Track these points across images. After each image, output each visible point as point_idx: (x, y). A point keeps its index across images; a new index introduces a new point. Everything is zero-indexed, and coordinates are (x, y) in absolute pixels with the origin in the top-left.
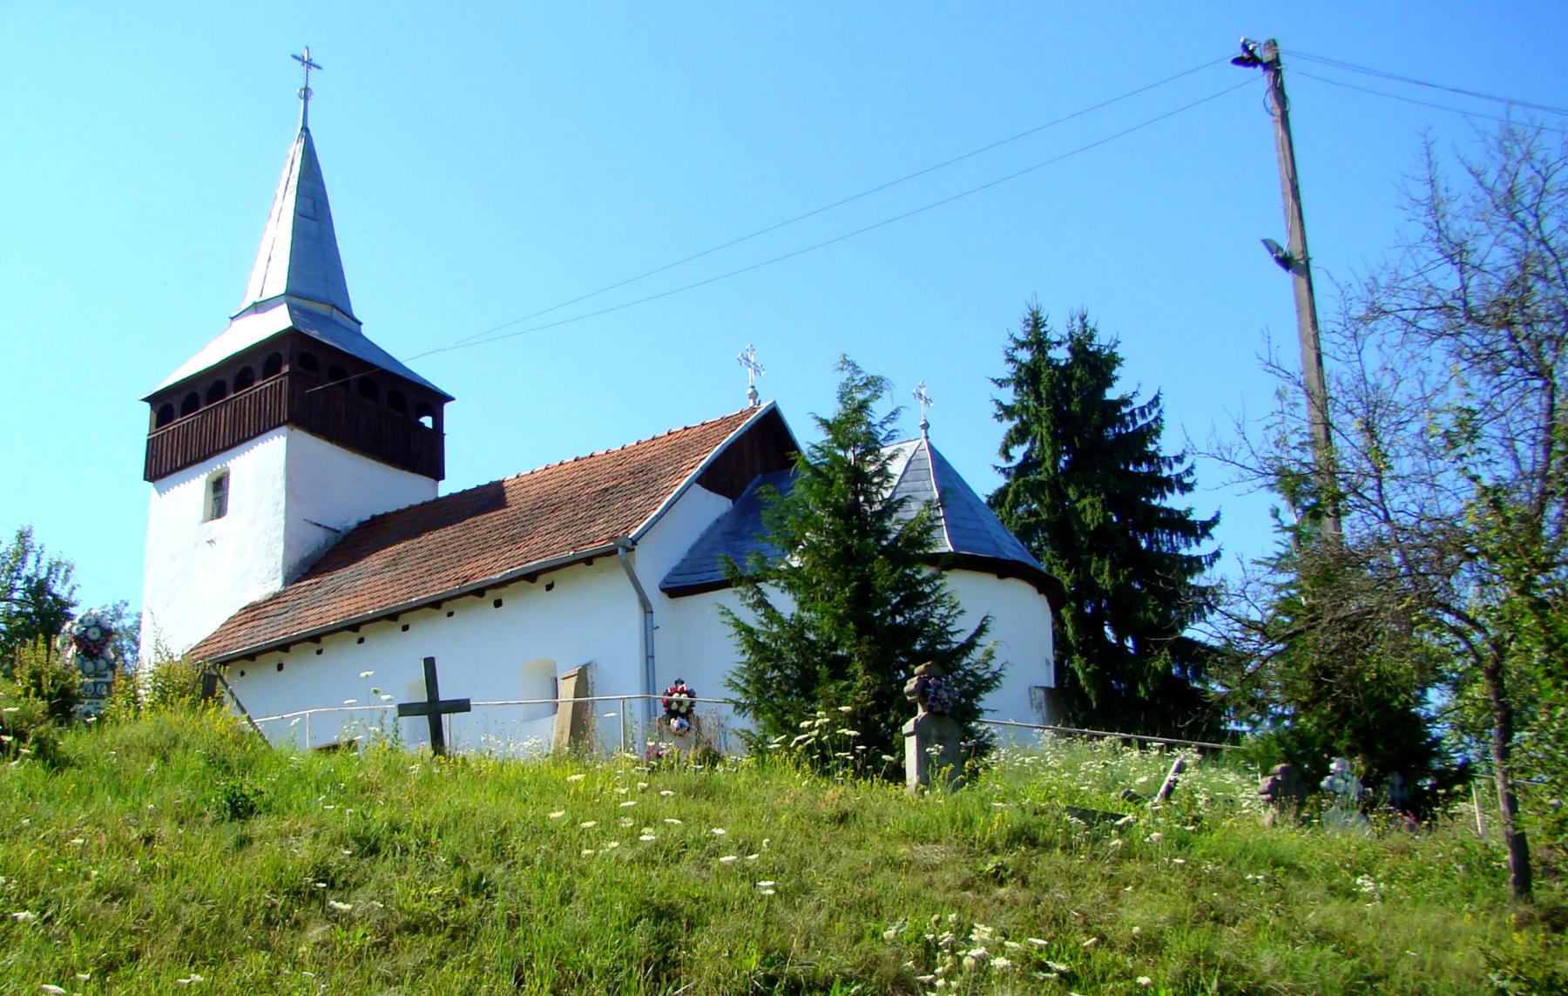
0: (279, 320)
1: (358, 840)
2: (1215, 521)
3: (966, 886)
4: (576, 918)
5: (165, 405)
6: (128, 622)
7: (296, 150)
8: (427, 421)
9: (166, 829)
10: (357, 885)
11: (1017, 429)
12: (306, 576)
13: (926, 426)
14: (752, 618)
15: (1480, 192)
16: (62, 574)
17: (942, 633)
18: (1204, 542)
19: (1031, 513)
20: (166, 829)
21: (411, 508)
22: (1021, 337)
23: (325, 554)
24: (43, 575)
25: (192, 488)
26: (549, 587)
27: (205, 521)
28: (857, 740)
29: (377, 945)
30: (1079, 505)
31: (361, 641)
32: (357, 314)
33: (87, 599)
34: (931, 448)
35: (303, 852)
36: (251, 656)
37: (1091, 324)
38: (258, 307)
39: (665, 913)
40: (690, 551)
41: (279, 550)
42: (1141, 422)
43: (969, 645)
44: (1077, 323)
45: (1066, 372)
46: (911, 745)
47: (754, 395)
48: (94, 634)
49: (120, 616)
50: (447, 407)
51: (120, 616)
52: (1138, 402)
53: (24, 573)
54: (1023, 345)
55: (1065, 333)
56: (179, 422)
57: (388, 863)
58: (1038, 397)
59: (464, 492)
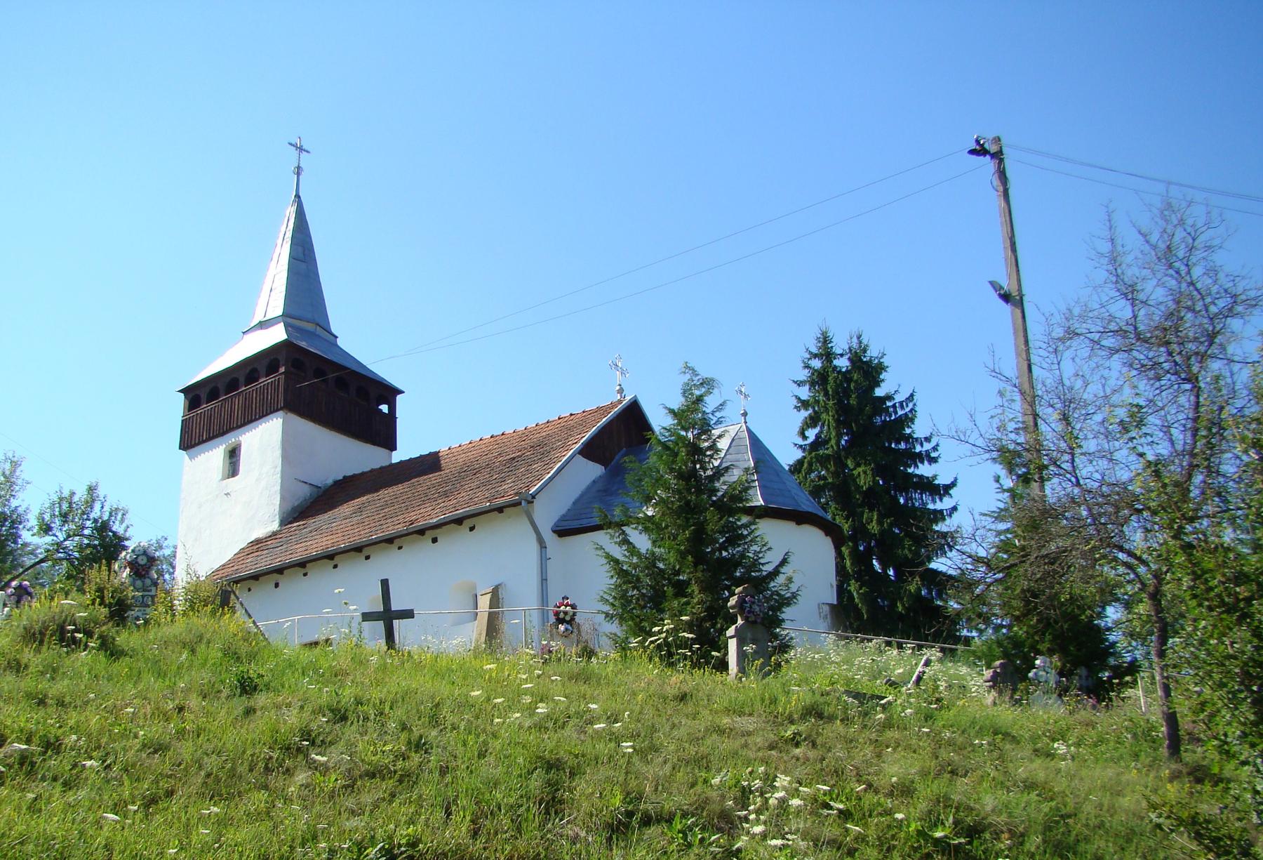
0: (278, 334)
1: (332, 711)
2: (953, 484)
3: (771, 747)
4: (490, 769)
5: (195, 395)
6: (167, 552)
7: (291, 211)
8: (384, 408)
9: (194, 702)
10: (331, 743)
11: (811, 417)
12: (296, 520)
13: (745, 414)
15: (1147, 248)
16: (119, 517)
18: (946, 499)
19: (820, 478)
20: (194, 702)
21: (372, 471)
22: (814, 350)
23: (309, 505)
24: (105, 518)
25: (215, 455)
26: (472, 529)
27: (223, 479)
28: (694, 641)
31: (335, 566)
32: (334, 330)
34: (749, 430)
35: (292, 719)
36: (255, 577)
37: (865, 342)
38: (263, 325)
39: (552, 765)
41: (277, 501)
42: (900, 412)
43: (775, 573)
44: (855, 340)
45: (846, 376)
46: (732, 645)
47: (621, 391)
48: (143, 561)
49: (161, 548)
50: (399, 397)
52: (899, 398)
53: (92, 516)
54: (815, 356)
56: (205, 407)
57: (354, 728)
58: (826, 394)
59: (411, 460)
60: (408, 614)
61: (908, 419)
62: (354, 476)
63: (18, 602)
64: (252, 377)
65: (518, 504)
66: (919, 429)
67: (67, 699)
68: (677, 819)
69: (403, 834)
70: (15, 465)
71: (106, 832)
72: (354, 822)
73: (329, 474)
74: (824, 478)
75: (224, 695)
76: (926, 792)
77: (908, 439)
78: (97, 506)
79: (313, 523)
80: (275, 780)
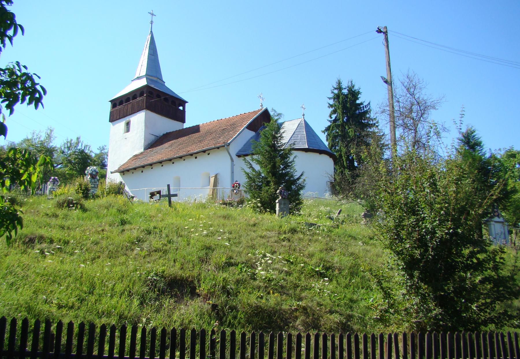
0: (143, 82)
1: (146, 230)
3: (276, 242)
4: (189, 249)
5: (115, 103)
6: (106, 151)
7: (149, 37)
8: (181, 108)
9: (107, 228)
10: (145, 241)
11: (334, 111)
12: (149, 148)
13: (304, 115)
14: (249, 171)
15: (403, 87)
16: (88, 148)
17: (292, 176)
19: (336, 132)
20: (107, 228)
21: (176, 131)
22: (335, 87)
23: (155, 142)
24: (83, 148)
25: (121, 124)
26: (209, 154)
27: (124, 133)
29: (148, 255)
30: (348, 131)
31: (162, 166)
32: (164, 80)
33: (94, 151)
34: (305, 121)
35: (135, 234)
36: (135, 169)
37: (353, 84)
38: (138, 78)
39: (209, 248)
40: (244, 146)
41: (143, 141)
42: (365, 109)
43: (298, 179)
44: (350, 83)
45: (346, 96)
46: (277, 205)
47: (262, 106)
48: (94, 173)
49: (104, 149)
50: (186, 104)
51: (104, 149)
52: (365, 104)
53: (78, 148)
54: (336, 89)
55: (347, 86)
56: (118, 107)
57: (153, 236)
58: (339, 103)
59: (190, 127)
60: (176, 195)
61: (366, 112)
62: (170, 133)
63: (54, 184)
64: (134, 97)
65: (224, 146)
66: (372, 115)
67: (71, 227)
68: (240, 265)
69: (160, 269)
70: (51, 131)
71: (81, 269)
72: (149, 265)
73: (161, 132)
74: (338, 133)
75: (116, 225)
76: (318, 256)
77: (369, 119)
78: (80, 145)
79: (155, 149)
80: (129, 252)
